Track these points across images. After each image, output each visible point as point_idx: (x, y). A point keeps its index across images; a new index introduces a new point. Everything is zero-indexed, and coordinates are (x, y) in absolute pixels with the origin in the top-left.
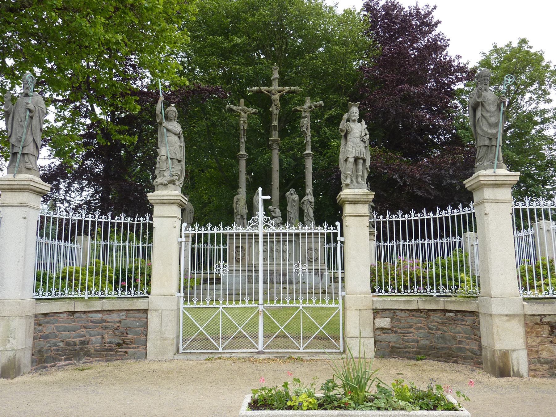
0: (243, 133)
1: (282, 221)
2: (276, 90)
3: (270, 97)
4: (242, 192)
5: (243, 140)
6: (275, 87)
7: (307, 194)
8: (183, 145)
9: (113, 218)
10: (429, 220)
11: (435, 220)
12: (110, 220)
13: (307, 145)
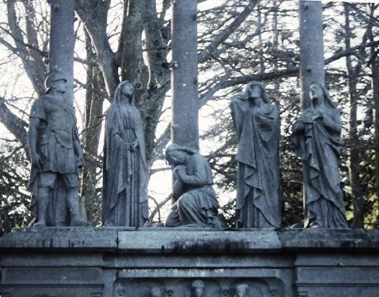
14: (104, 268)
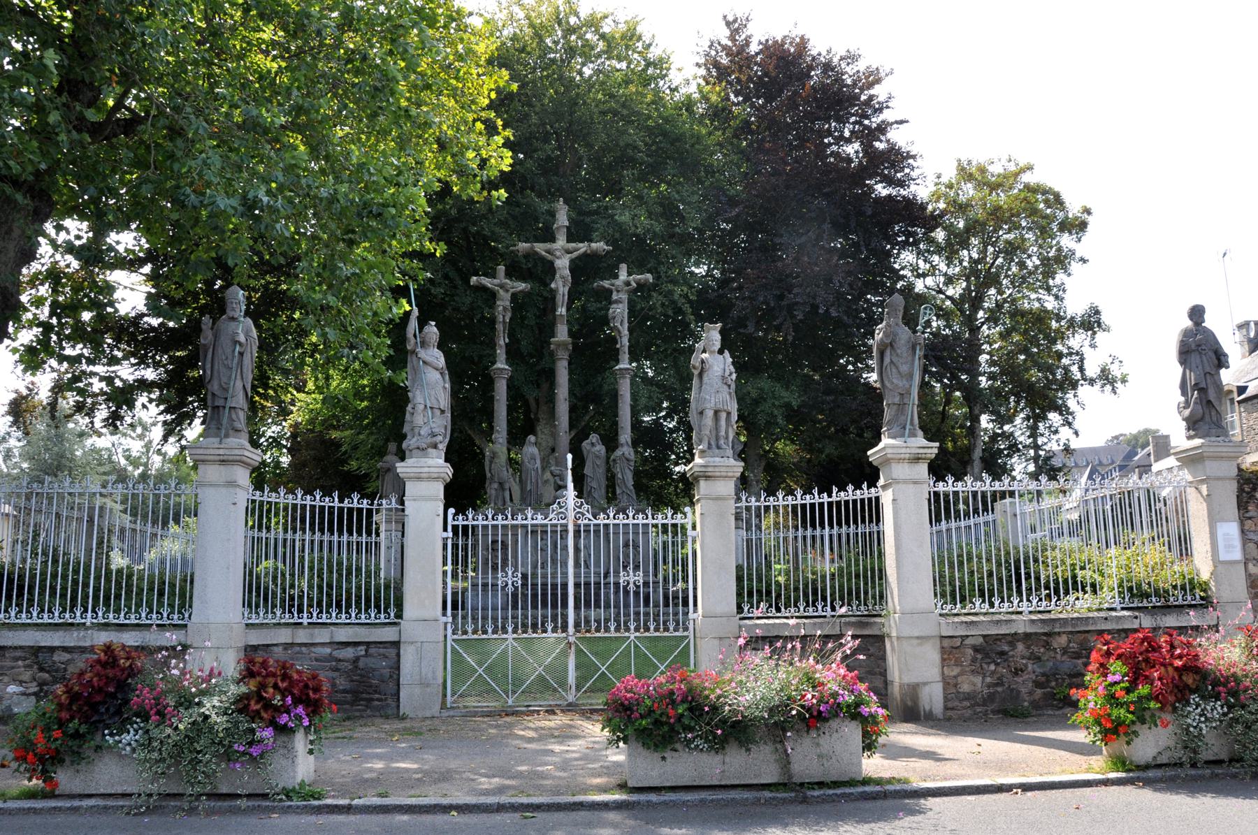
2: (562, 254)
3: (552, 263)
5: (502, 342)
6: (561, 242)
8: (448, 385)
9: (341, 501)
10: (821, 505)
12: (336, 504)
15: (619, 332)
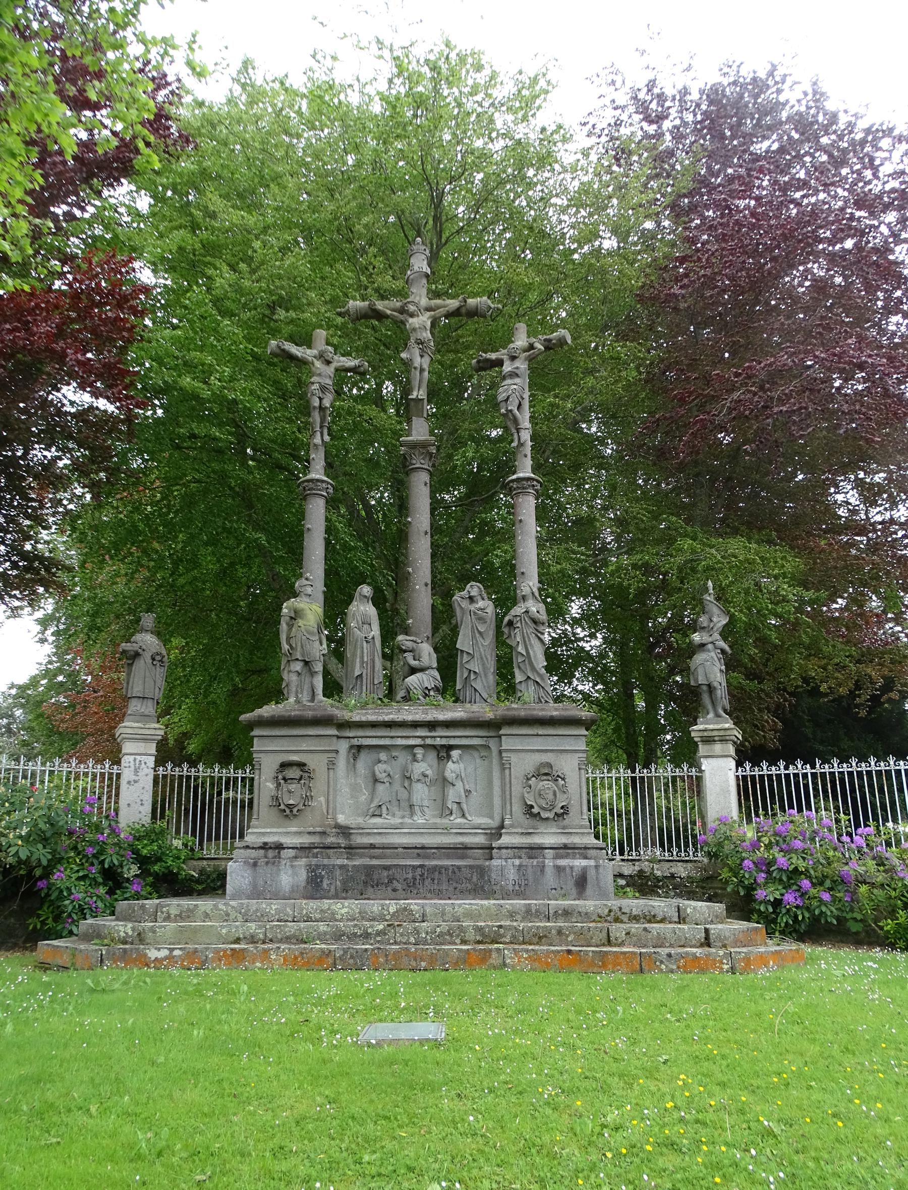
0: (318, 420)
1: (440, 685)
4: (309, 590)
7: (524, 598)
10: (805, 776)
11: (814, 775)
13: (519, 456)
14: (338, 737)
15: (516, 421)
